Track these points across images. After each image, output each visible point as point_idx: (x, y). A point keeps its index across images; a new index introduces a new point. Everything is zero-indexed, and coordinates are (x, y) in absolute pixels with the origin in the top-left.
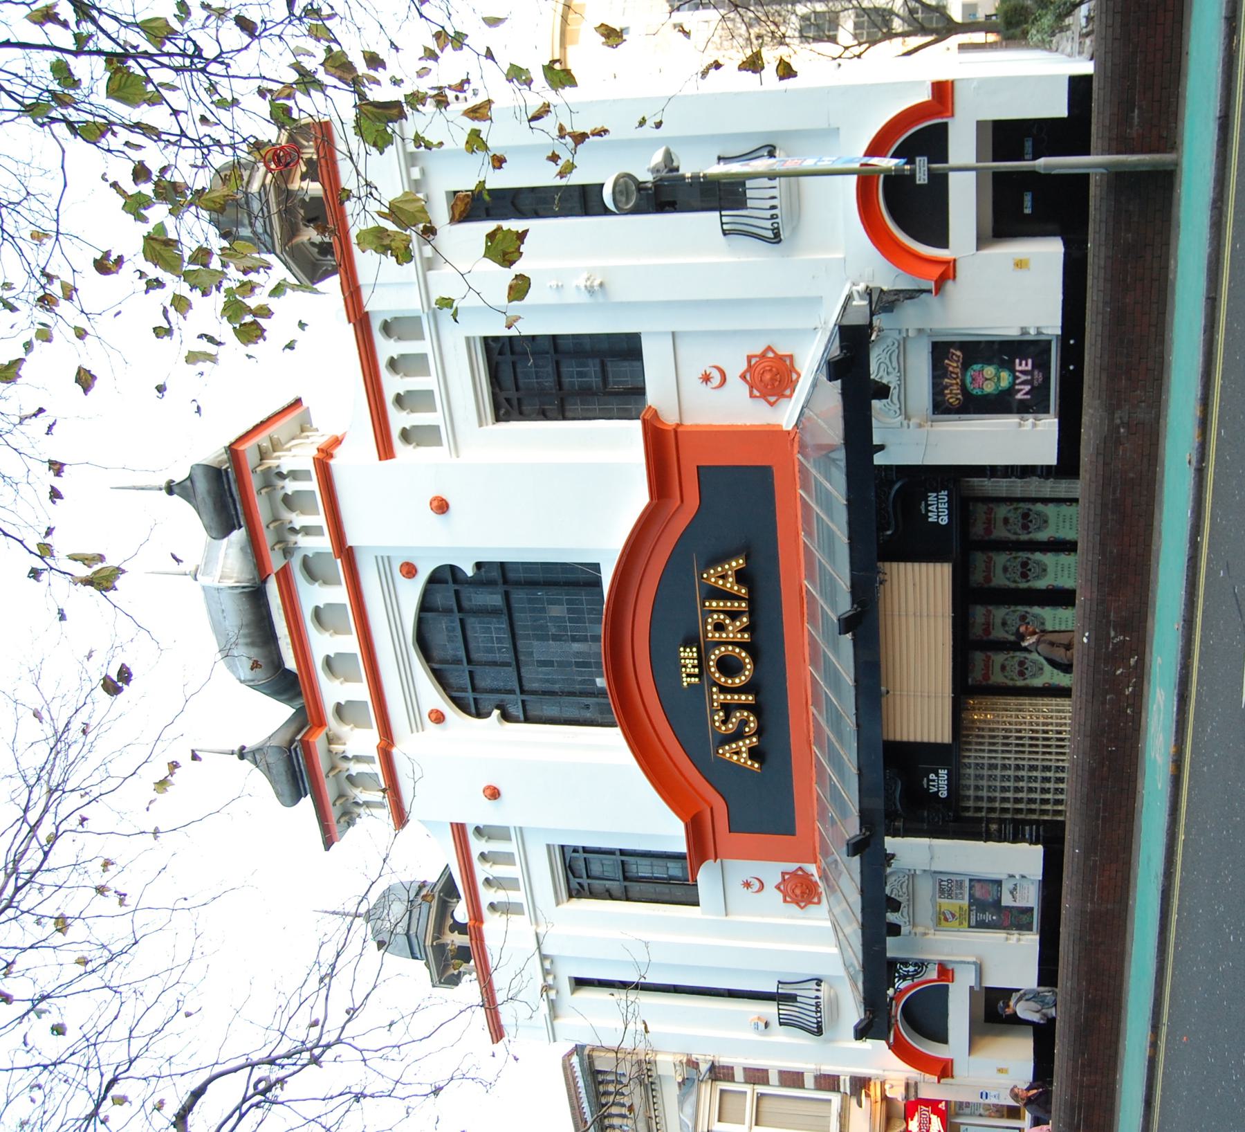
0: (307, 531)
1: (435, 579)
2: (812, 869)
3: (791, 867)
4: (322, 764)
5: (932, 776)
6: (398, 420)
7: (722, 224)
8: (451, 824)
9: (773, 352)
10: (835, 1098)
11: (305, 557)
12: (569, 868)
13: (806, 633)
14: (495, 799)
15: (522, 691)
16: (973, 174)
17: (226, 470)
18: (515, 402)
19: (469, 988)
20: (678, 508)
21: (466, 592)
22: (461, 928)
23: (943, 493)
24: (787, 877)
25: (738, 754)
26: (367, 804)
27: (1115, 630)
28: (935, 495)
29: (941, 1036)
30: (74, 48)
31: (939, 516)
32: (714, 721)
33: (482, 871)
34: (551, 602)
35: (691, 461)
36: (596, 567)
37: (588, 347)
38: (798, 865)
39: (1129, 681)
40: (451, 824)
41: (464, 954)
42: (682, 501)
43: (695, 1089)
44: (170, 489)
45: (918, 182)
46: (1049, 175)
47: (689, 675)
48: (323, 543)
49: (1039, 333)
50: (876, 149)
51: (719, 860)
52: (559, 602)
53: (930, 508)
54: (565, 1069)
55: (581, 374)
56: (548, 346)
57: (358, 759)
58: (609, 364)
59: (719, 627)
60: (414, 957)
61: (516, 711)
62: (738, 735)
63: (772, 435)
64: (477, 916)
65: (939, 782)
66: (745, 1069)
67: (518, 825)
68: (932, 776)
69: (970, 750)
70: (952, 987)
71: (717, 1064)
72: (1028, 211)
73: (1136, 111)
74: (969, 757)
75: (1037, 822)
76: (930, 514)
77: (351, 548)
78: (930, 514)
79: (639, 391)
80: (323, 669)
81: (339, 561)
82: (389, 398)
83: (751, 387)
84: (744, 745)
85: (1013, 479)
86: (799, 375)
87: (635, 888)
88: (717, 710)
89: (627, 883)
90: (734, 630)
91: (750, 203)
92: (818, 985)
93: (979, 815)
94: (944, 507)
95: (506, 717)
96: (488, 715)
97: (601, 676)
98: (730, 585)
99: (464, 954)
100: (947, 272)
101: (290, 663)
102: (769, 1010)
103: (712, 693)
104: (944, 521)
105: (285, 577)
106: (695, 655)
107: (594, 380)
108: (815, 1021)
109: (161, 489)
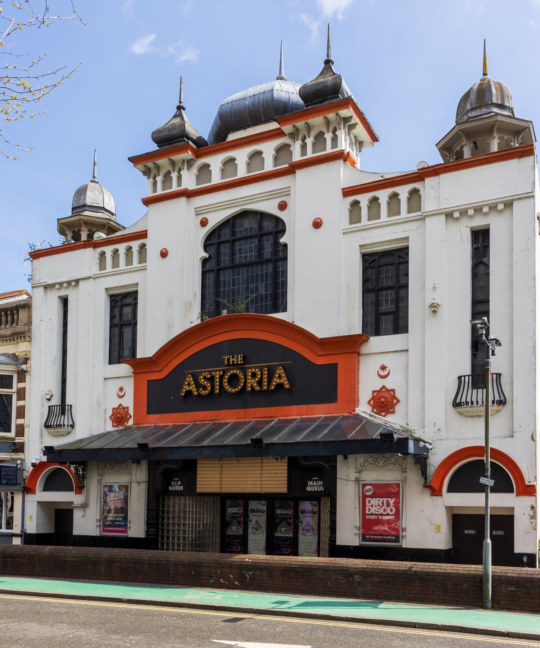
0: (304, 147)
1: (279, 221)
2: (131, 422)
3: (131, 412)
4: (178, 157)
5: (179, 483)
6: (364, 199)
7: (465, 376)
8: (147, 230)
9: (397, 403)
10: (12, 434)
11: (289, 146)
12: (125, 295)
13: (251, 420)
14: (161, 255)
15: (219, 270)
16: (484, 505)
17: (339, 97)
18: (372, 265)
19: (58, 240)
20: (316, 354)
21: (271, 238)
22: (90, 236)
23: (323, 488)
24: (126, 410)
25: (189, 385)
26: (155, 183)
27: (252, 574)
28: (322, 484)
29: (47, 488)
30: (457, 402)
31: (311, 486)
32: (205, 372)
33: (122, 247)
34: (266, 285)
35: (339, 360)
36: (285, 310)
37: (401, 305)
38: (132, 414)
39: (226, 581)
40: (147, 230)
41: (77, 237)
42: (319, 356)
43: (12, 362)
44: (328, 62)
45: (482, 478)
46: (482, 545)
47: (228, 359)
48: (297, 157)
49: (403, 537)
50: (496, 453)
51: (133, 375)
52: (266, 290)
53: (315, 482)
54: (20, 291)
55: (387, 301)
56: (402, 282)
57: (179, 178)
58: (392, 316)
59: (254, 375)
60: (73, 209)
61: (208, 266)
62: (198, 385)
63: (354, 402)
64: (96, 245)
65: (177, 486)
66: (25, 388)
67: (148, 267)
68: (179, 483)
69: (193, 501)
70: (72, 493)
71: (26, 374)
72: (466, 532)
73: (514, 589)
74: (190, 501)
75: (157, 535)
76: (312, 482)
77: (295, 173)
78: (312, 482)
79: (378, 333)
80: (228, 157)
81: (287, 165)
82: (396, 189)
83: (378, 391)
84: (193, 388)
85: (329, 523)
86: (384, 416)
87: (116, 330)
88: (211, 375)
89: (119, 326)
90: (252, 383)
91: (475, 391)
92: (71, 426)
93: (161, 506)
94: (316, 489)
95: (204, 262)
96: (206, 251)
97: (228, 313)
98: (276, 381)
99: (77, 237)
100: (436, 492)
101: (232, 137)
102: (56, 401)
103: (219, 371)
104: (309, 489)
105: (278, 133)
106: (239, 362)
107: (383, 308)
108: (52, 424)
109: (328, 56)
